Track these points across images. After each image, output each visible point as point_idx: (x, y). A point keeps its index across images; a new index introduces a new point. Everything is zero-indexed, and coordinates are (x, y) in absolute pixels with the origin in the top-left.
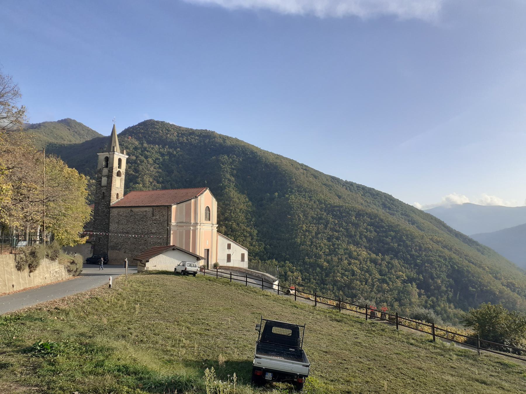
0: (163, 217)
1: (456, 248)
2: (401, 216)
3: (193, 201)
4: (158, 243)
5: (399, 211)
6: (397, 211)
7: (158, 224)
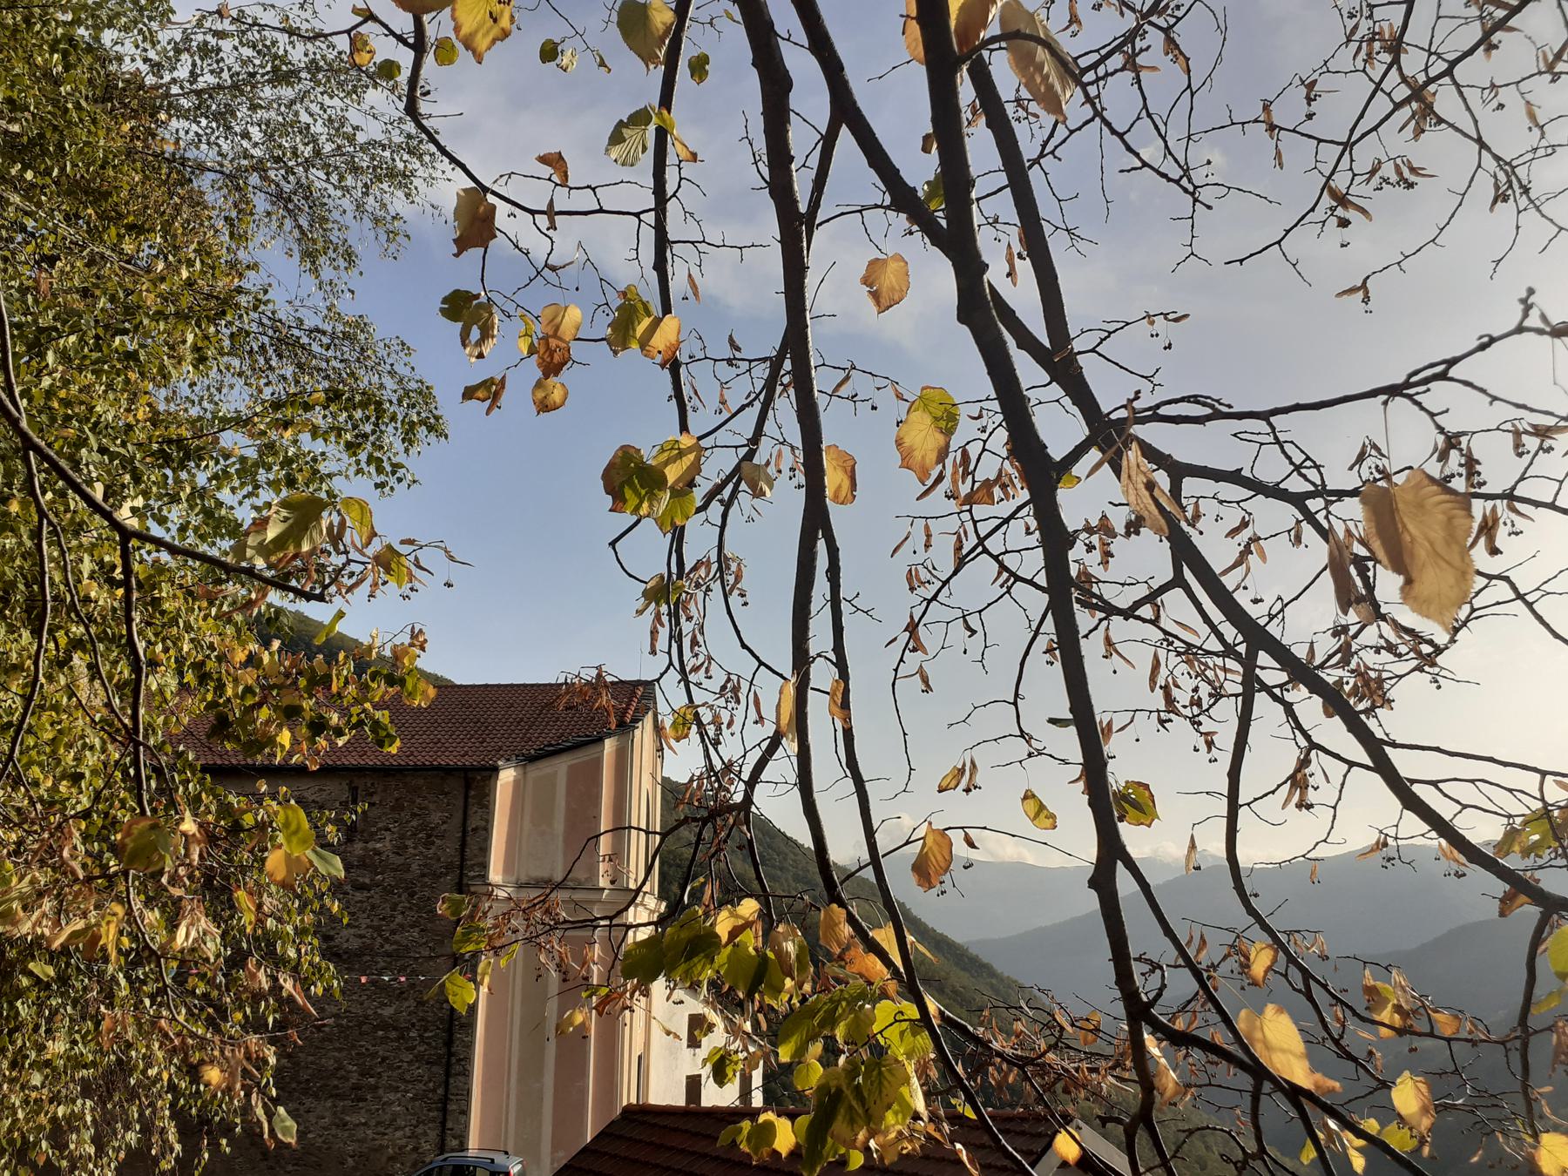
0: (428, 844)
1: (953, 987)
2: (793, 884)
3: (609, 745)
4: (376, 1028)
5: (788, 870)
6: (781, 869)
7: (388, 891)
